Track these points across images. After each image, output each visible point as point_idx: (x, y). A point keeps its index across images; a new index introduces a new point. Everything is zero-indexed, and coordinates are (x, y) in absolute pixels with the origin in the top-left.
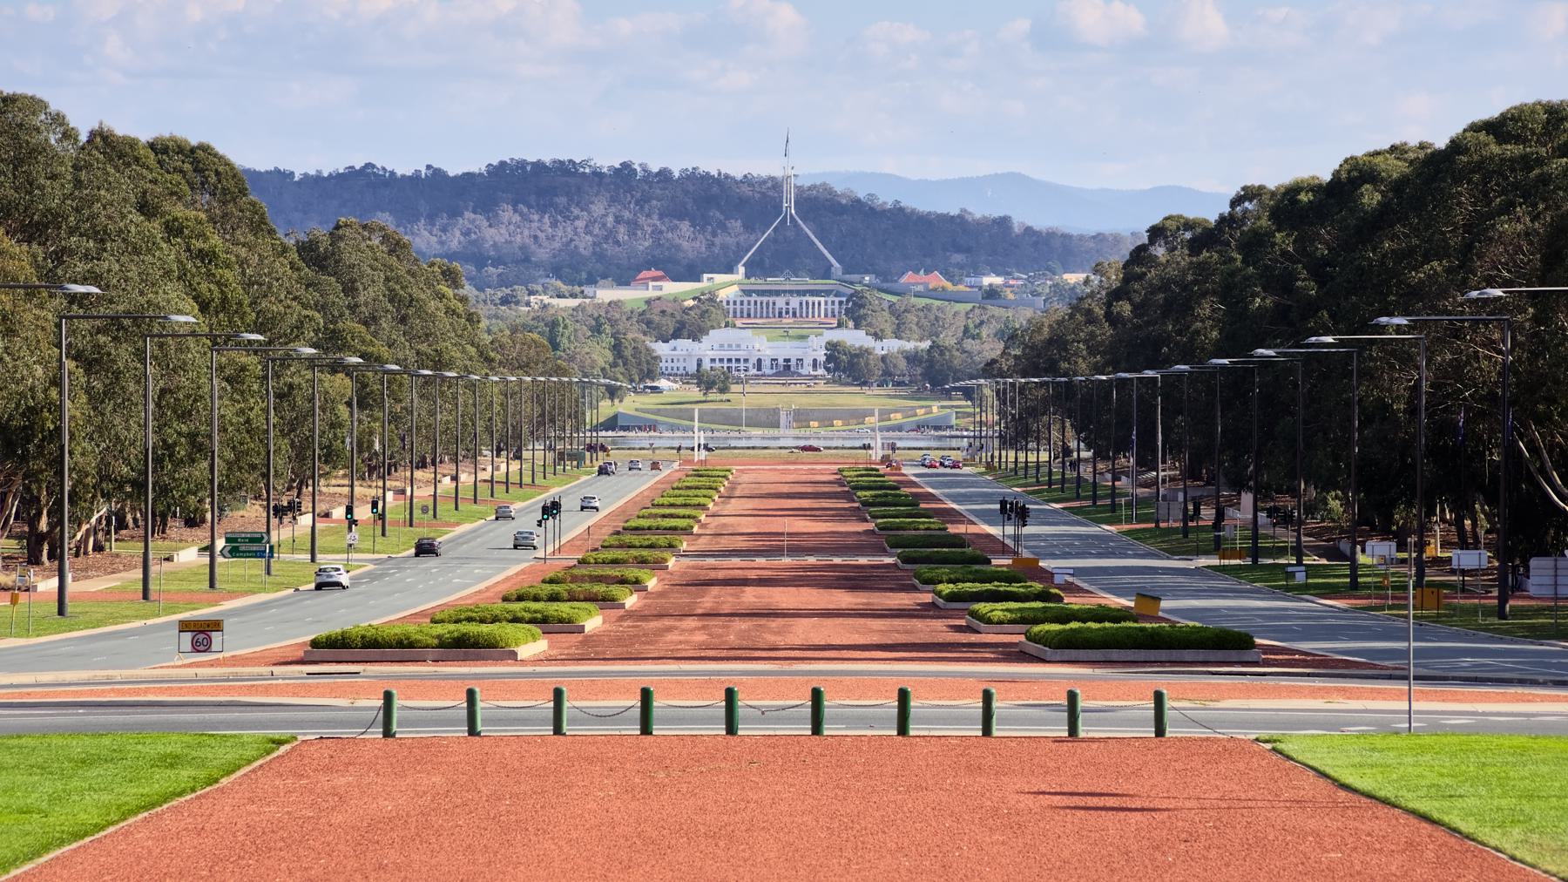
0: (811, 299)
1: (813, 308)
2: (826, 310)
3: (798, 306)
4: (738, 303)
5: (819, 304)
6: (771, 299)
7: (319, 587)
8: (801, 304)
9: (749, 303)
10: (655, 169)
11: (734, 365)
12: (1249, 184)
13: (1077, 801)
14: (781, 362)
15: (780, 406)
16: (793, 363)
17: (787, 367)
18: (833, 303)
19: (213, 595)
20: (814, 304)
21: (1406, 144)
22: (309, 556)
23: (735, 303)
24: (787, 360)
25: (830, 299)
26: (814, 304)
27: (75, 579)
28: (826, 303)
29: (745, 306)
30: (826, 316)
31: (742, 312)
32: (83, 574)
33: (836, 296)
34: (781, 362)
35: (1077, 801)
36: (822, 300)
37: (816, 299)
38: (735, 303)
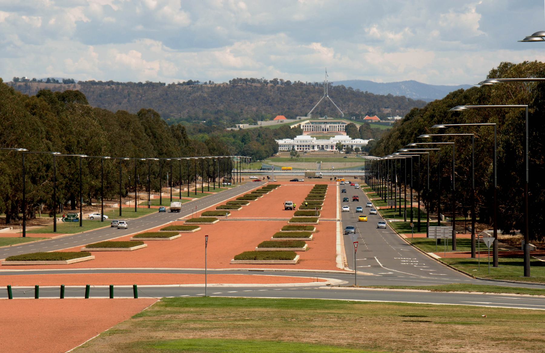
0: (333, 125)
1: (334, 128)
2: (338, 128)
3: (329, 127)
4: (304, 126)
5: (336, 127)
6: (320, 125)
7: (160, 212)
8: (330, 127)
9: (308, 126)
10: (285, 81)
11: (305, 148)
12: (448, 94)
13: (420, 319)
14: (320, 146)
15: (271, 178)
16: (325, 147)
17: (323, 148)
18: (341, 126)
19: (82, 228)
20: (334, 127)
21: (198, 82)
22: (179, 197)
23: (306, 126)
24: (323, 146)
25: (340, 125)
26: (334, 127)
27: (84, 214)
28: (338, 126)
29: (307, 127)
30: (338, 130)
31: (310, 129)
32: (86, 211)
33: (342, 124)
34: (320, 146)
35: (420, 319)
36: (337, 125)
37: (335, 125)
38: (306, 126)
